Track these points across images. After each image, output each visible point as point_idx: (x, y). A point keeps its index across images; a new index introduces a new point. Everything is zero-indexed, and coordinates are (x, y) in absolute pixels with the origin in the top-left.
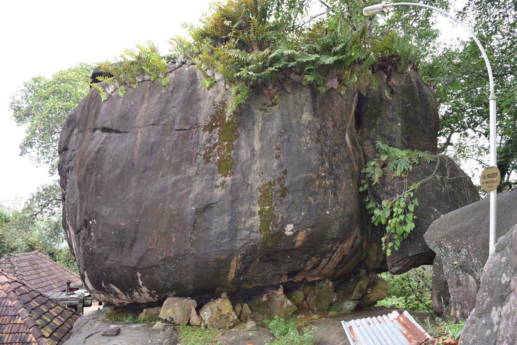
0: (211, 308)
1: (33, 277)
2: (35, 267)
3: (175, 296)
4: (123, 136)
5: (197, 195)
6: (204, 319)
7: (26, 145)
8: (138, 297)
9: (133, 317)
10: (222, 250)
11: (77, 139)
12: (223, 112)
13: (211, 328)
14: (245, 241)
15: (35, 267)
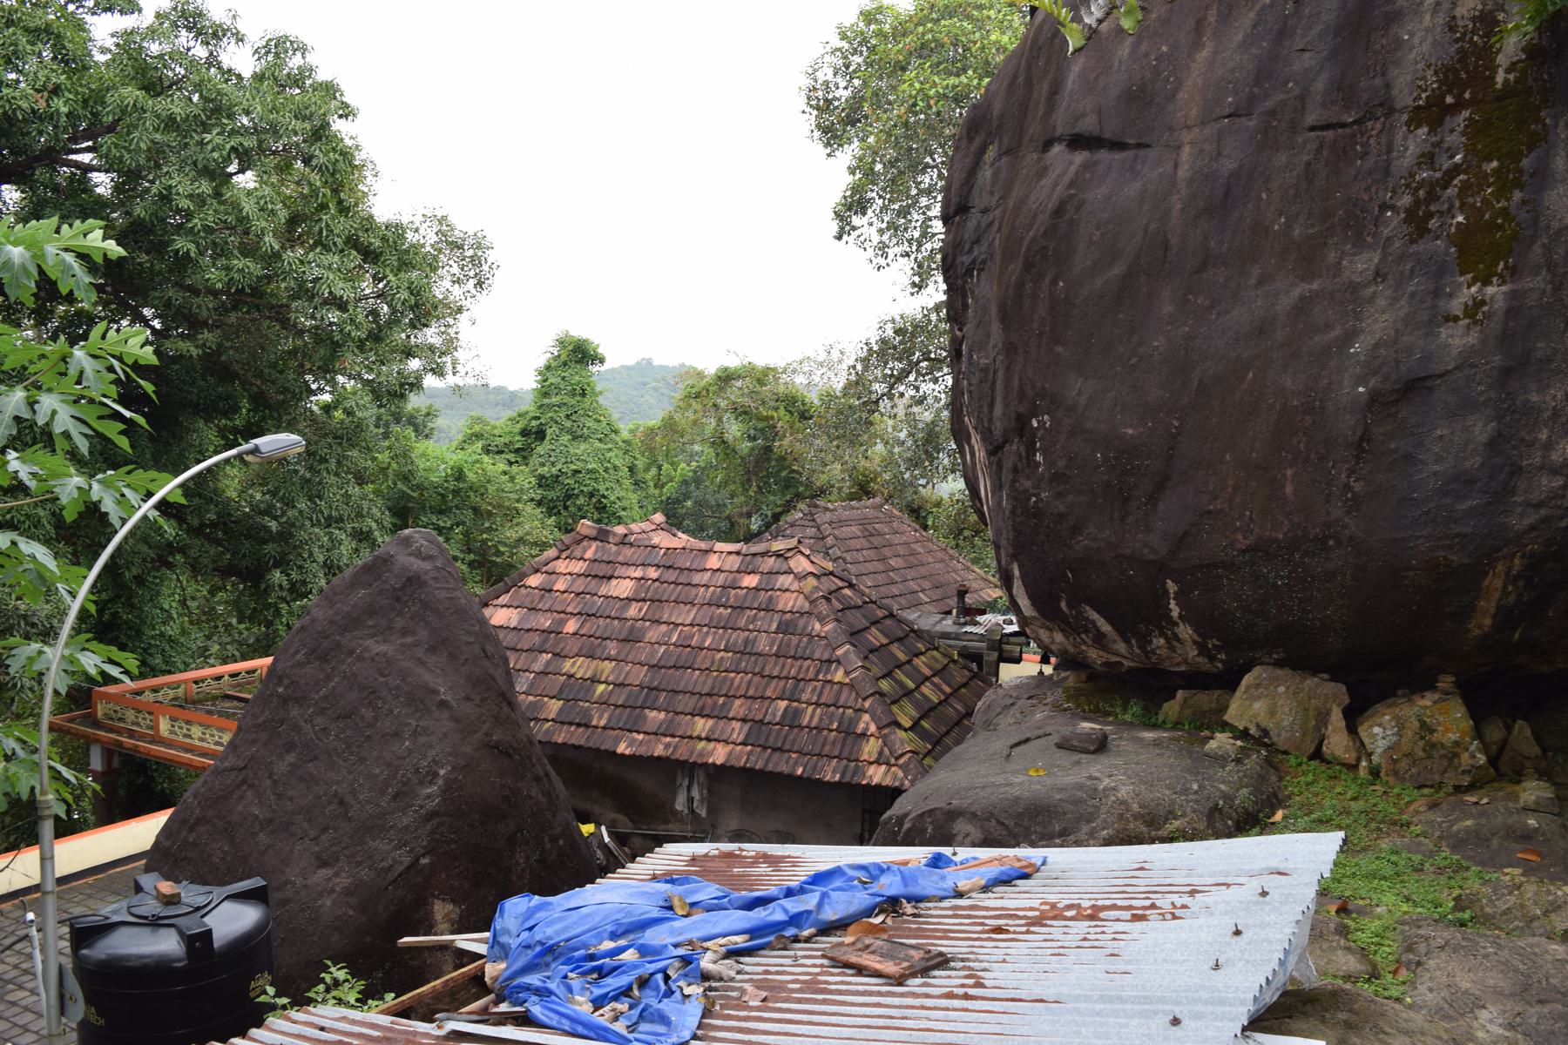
1: (870, 567)
2: (876, 541)
3: (1279, 664)
4: (1136, 157)
5: (1377, 346)
6: (1369, 747)
7: (850, 209)
8: (1164, 652)
9: (1145, 708)
10: (1457, 535)
11: (996, 174)
12: (1487, 54)
13: (1391, 780)
14: (1543, 512)
15: (876, 541)
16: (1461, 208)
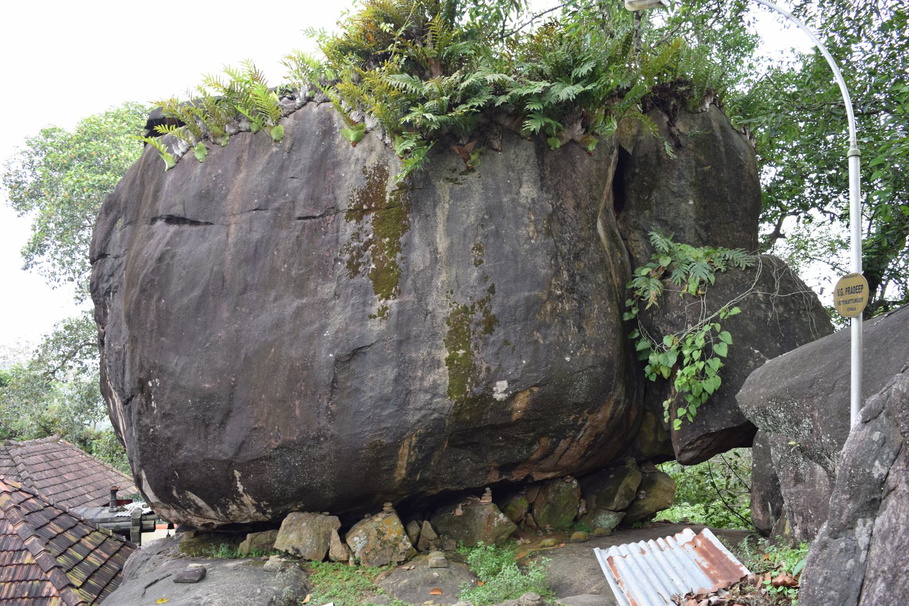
0: (365, 530)
1: (51, 481)
2: (54, 464)
3: (302, 510)
4: (205, 230)
5: (337, 332)
6: (353, 549)
7: (32, 251)
8: (236, 513)
9: (230, 548)
10: (384, 428)
11: (123, 236)
12: (381, 185)
13: (366, 565)
14: (423, 412)
15: (54, 464)
16: (373, 261)
